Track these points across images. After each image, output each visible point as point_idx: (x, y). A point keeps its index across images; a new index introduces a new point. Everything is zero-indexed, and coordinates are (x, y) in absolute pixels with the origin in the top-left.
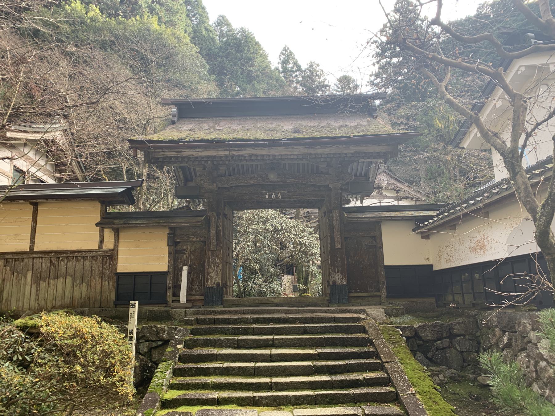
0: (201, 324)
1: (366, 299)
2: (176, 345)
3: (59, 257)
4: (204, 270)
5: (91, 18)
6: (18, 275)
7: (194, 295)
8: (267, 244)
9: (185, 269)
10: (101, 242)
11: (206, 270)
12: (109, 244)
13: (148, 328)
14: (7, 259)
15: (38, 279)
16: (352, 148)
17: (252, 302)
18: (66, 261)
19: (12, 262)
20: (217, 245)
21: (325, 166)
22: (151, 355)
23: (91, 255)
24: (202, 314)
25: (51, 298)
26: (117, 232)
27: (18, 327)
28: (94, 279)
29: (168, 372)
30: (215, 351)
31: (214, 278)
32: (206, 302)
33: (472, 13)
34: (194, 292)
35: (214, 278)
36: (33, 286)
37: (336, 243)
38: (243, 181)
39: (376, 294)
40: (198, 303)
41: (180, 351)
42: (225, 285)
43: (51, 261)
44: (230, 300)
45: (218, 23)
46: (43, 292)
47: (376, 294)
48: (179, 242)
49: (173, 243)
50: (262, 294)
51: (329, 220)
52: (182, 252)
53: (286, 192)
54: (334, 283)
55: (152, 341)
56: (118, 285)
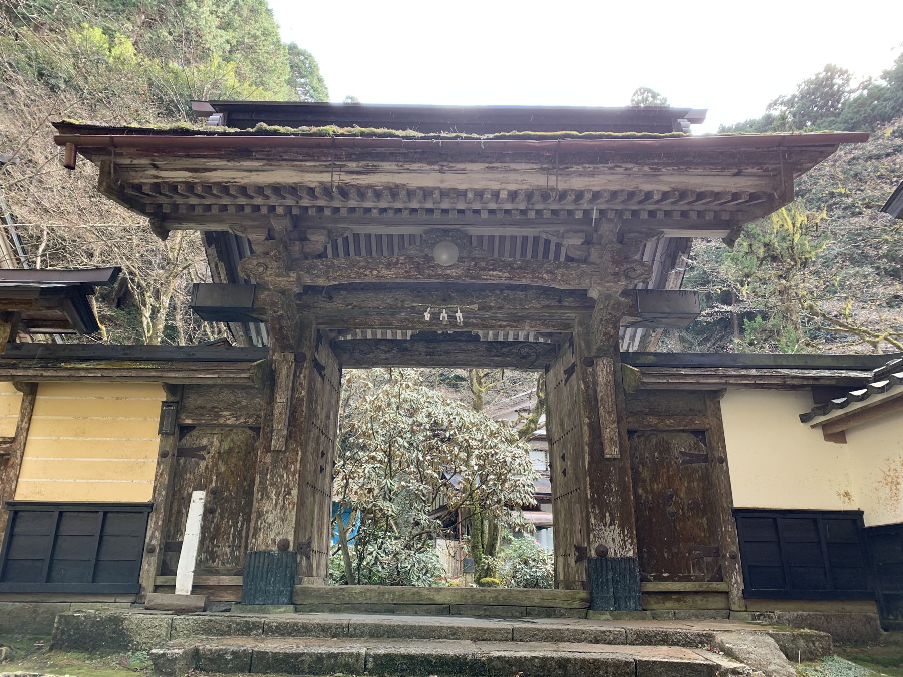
1: (689, 599)
4: (250, 503)
7: (217, 573)
8: (417, 457)
9: (198, 499)
11: (255, 504)
16: (665, 178)
17: (374, 600)
20: (290, 437)
26: (30, 390)
31: (275, 527)
32: (249, 595)
33: (758, 114)
34: (217, 564)
37: (606, 443)
38: (367, 272)
39: (716, 586)
42: (304, 548)
44: (314, 590)
47: (716, 586)
48: (191, 428)
49: (177, 429)
50: (400, 578)
51: (586, 383)
53: (475, 307)
54: (602, 552)
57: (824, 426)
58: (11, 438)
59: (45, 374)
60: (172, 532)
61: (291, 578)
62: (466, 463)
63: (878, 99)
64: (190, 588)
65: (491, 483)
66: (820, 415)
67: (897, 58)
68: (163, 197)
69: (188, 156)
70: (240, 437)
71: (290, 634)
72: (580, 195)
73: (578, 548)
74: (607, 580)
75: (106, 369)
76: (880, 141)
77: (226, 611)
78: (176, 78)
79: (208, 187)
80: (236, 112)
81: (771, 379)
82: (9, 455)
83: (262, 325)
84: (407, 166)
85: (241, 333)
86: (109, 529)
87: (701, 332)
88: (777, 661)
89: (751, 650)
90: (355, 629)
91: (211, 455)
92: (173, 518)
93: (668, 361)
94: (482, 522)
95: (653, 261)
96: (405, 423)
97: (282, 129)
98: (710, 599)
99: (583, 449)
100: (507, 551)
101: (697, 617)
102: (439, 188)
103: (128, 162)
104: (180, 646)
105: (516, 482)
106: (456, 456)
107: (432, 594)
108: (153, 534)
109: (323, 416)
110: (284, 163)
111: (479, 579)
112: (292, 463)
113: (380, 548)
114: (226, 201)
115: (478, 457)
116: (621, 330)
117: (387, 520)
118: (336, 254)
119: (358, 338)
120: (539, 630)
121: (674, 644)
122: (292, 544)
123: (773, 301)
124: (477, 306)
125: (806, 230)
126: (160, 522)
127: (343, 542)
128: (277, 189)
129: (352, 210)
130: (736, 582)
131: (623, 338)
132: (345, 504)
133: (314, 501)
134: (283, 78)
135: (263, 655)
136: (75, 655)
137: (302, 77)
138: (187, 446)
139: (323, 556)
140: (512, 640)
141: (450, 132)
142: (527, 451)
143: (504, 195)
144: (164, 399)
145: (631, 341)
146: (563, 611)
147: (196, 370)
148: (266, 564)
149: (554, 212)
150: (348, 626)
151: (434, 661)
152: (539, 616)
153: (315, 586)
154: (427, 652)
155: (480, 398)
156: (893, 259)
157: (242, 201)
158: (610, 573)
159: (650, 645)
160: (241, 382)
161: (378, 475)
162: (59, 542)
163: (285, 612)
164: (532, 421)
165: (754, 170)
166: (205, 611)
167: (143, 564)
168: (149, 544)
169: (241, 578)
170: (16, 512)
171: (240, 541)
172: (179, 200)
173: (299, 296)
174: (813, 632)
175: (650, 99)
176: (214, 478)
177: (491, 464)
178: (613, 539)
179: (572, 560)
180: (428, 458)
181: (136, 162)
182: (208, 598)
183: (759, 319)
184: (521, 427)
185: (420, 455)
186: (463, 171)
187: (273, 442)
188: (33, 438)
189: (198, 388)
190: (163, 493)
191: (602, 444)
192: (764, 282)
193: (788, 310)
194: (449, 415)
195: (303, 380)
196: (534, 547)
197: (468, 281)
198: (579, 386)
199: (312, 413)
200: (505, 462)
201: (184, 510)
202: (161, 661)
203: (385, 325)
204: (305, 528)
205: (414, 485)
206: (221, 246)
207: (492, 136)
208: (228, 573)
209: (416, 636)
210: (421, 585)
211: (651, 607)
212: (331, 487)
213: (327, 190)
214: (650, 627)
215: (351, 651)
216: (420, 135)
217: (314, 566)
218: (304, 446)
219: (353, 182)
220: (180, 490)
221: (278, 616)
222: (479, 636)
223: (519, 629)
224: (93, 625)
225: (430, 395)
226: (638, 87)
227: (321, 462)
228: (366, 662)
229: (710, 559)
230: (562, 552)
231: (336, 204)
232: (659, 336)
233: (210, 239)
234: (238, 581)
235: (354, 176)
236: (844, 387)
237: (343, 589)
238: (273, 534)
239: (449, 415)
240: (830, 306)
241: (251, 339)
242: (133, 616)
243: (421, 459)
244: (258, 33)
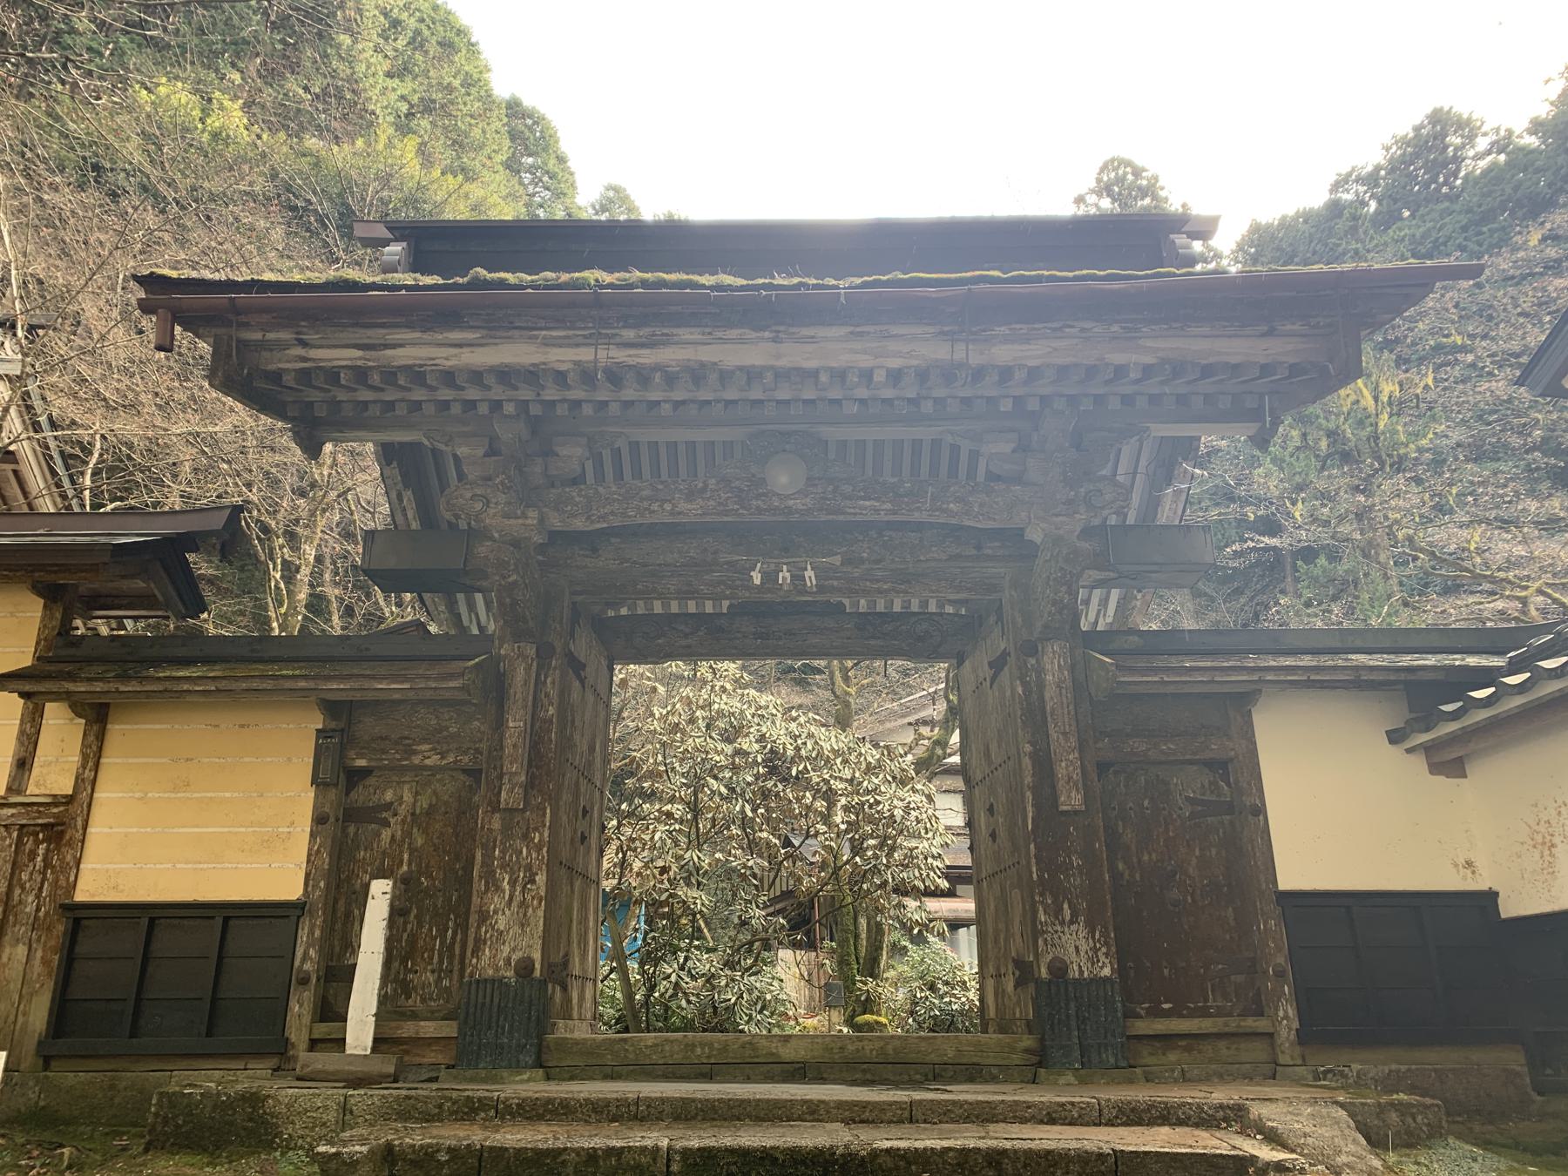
4: (466, 899)
5: (215, 136)
7: (415, 1016)
8: (743, 811)
9: (380, 893)
10: (23, 764)
11: (476, 900)
12: (54, 774)
16: (1150, 343)
17: (678, 1058)
20: (530, 786)
21: (1007, 448)
26: (97, 716)
31: (510, 938)
32: (469, 1053)
33: (1317, 198)
34: (414, 1002)
35: (510, 938)
38: (655, 507)
39: (1251, 1023)
40: (431, 1057)
42: (558, 972)
44: (576, 1042)
45: (602, 206)
47: (1251, 1023)
48: (366, 772)
50: (718, 1018)
51: (1025, 684)
52: (375, 815)
54: (1059, 969)
56: (69, 959)
57: (1428, 749)
59: (122, 688)
60: (337, 949)
62: (826, 818)
63: (1525, 170)
64: (370, 1044)
65: (870, 853)
66: (1421, 731)
67: (1554, 97)
68: (317, 393)
69: (356, 325)
71: (540, 1118)
72: (1006, 373)
73: (1019, 964)
74: (1068, 1016)
75: (224, 678)
76: (1521, 254)
77: (430, 1080)
78: (317, 165)
79: (390, 375)
80: (434, 242)
81: (1332, 674)
82: (63, 824)
83: (479, 597)
84: (720, 334)
85: (442, 608)
87: (1226, 580)
88: (1352, 1147)
89: (1307, 1130)
90: (649, 1106)
93: (1169, 642)
94: (855, 919)
95: (1135, 473)
96: (720, 753)
97: (510, 277)
98: (1242, 1046)
99: (1023, 796)
100: (900, 968)
101: (1221, 1077)
102: (772, 367)
103: (258, 336)
104: (363, 1141)
105: (911, 850)
106: (808, 808)
107: (775, 1047)
108: (306, 954)
109: (585, 748)
110: (516, 333)
111: (852, 1017)
112: (536, 829)
113: (682, 969)
114: (418, 395)
115: (846, 809)
116: (1082, 593)
117: (694, 921)
118: (600, 478)
119: (640, 612)
120: (954, 1103)
121: (1181, 1123)
122: (538, 966)
123: (1344, 529)
124: (839, 557)
125: (1398, 407)
126: (317, 933)
127: (619, 957)
128: (505, 375)
129: (628, 404)
130: (1286, 1017)
131: (1087, 602)
132: (622, 893)
134: (499, 158)
137: (530, 155)
138: (359, 804)
139: (590, 985)
140: (911, 1121)
141: (790, 275)
142: (930, 799)
143: (880, 376)
144: (320, 726)
145: (1099, 611)
146: (995, 1071)
147: (373, 677)
148: (496, 1000)
149: (966, 401)
150: (638, 1101)
151: (781, 1157)
152: (954, 1080)
153: (577, 1035)
154: (769, 1143)
155: (847, 705)
156: (1557, 452)
157: (445, 394)
158: (1072, 1005)
159: (1140, 1124)
160: (447, 695)
161: (676, 843)
162: (150, 969)
163: (529, 1080)
164: (937, 743)
165: (1295, 327)
166: (396, 1081)
168: (300, 969)
169: (454, 1024)
170: (77, 921)
171: (451, 963)
172: (342, 396)
173: (541, 548)
174: (1414, 1099)
175: (1130, 177)
176: (406, 856)
177: (871, 820)
178: (1077, 948)
179: (1010, 985)
180: (761, 811)
181: (271, 336)
183: (1322, 561)
184: (920, 751)
185: (748, 808)
186: (812, 340)
189: (376, 706)
190: (322, 884)
191: (1054, 787)
192: (1326, 497)
193: (1370, 543)
194: (795, 738)
195: (551, 689)
196: (942, 961)
197: (824, 518)
198: (1013, 690)
200: (892, 816)
201: (356, 912)
202: (333, 1165)
203: (684, 596)
205: (739, 859)
206: (402, 464)
207: (858, 281)
210: (754, 1030)
211: (1144, 1061)
212: (599, 864)
213: (587, 375)
214: (1140, 1094)
215: (644, 1143)
216: (741, 282)
217: (575, 1001)
219: (631, 361)
220: (349, 879)
221: (520, 1087)
222: (855, 1115)
223: (920, 1102)
224: (215, 1107)
225: (763, 703)
226: (1108, 157)
227: (582, 825)
228: (669, 1160)
229: (1240, 978)
230: (992, 970)
231: (602, 396)
232: (1148, 597)
233: (388, 454)
234: (449, 1029)
235: (632, 352)
236: (1459, 683)
237: (625, 1040)
239: (795, 738)
240: (1447, 536)
241: (459, 616)
242: (284, 1092)
243: (750, 814)
244: (456, 83)
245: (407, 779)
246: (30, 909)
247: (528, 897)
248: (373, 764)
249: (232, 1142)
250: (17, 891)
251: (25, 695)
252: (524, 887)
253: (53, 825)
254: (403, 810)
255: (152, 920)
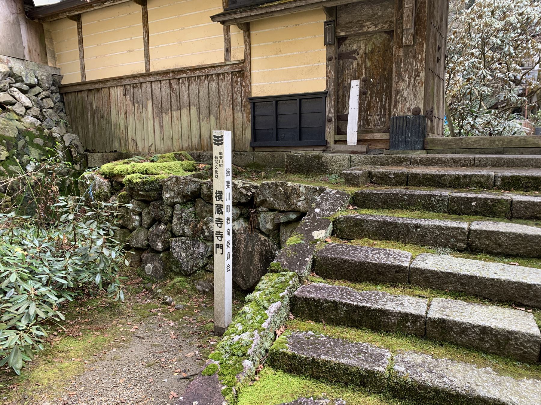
0: (378, 184)
2: (311, 231)
3: (179, 79)
4: (390, 86)
6: (139, 105)
7: (372, 132)
9: (355, 86)
10: (228, 50)
11: (394, 85)
12: (238, 55)
13: (270, 188)
14: (125, 85)
15: (160, 111)
17: (487, 146)
18: (187, 85)
19: (131, 89)
20: (416, 34)
22: (278, 236)
23: (216, 72)
24: (383, 164)
25: (177, 138)
26: (247, 28)
27: (103, 174)
28: (224, 109)
29: (274, 307)
30: (404, 256)
31: (409, 99)
32: (393, 144)
34: (372, 127)
35: (409, 99)
36: (155, 120)
40: (379, 146)
41: (319, 247)
43: (171, 86)
46: (167, 129)
48: (344, 38)
49: (335, 41)
55: (281, 212)
58: (242, 60)
59: (252, 14)
60: (341, 109)
61: (423, 133)
64: (356, 141)
70: (378, 40)
82: (244, 70)
86: (304, 109)
90: (480, 161)
91: (360, 56)
92: (340, 100)
108: (329, 110)
109: (439, 18)
112: (419, 53)
122: (422, 111)
126: (333, 103)
133: (434, 82)
135: (416, 175)
136: (299, 176)
138: (344, 51)
139: (441, 121)
144: (325, 21)
148: (405, 125)
162: (279, 119)
163: (420, 154)
167: (326, 129)
168: (328, 117)
169: (388, 134)
170: (254, 103)
171: (385, 112)
182: (368, 147)
187: (404, 39)
188: (254, 58)
190: (333, 84)
199: (431, 15)
201: (346, 94)
202: (350, 177)
204: (429, 101)
208: (379, 131)
209: (532, 166)
217: (436, 127)
218: (426, 39)
220: (342, 82)
228: (495, 180)
234: (386, 136)
238: (408, 105)
245: (362, 39)
246: (240, 100)
247: (417, 83)
248: (347, 34)
249: (312, 171)
250: (235, 95)
251: (223, 23)
252: (415, 78)
253: (241, 71)
254: (361, 52)
255: (277, 102)
